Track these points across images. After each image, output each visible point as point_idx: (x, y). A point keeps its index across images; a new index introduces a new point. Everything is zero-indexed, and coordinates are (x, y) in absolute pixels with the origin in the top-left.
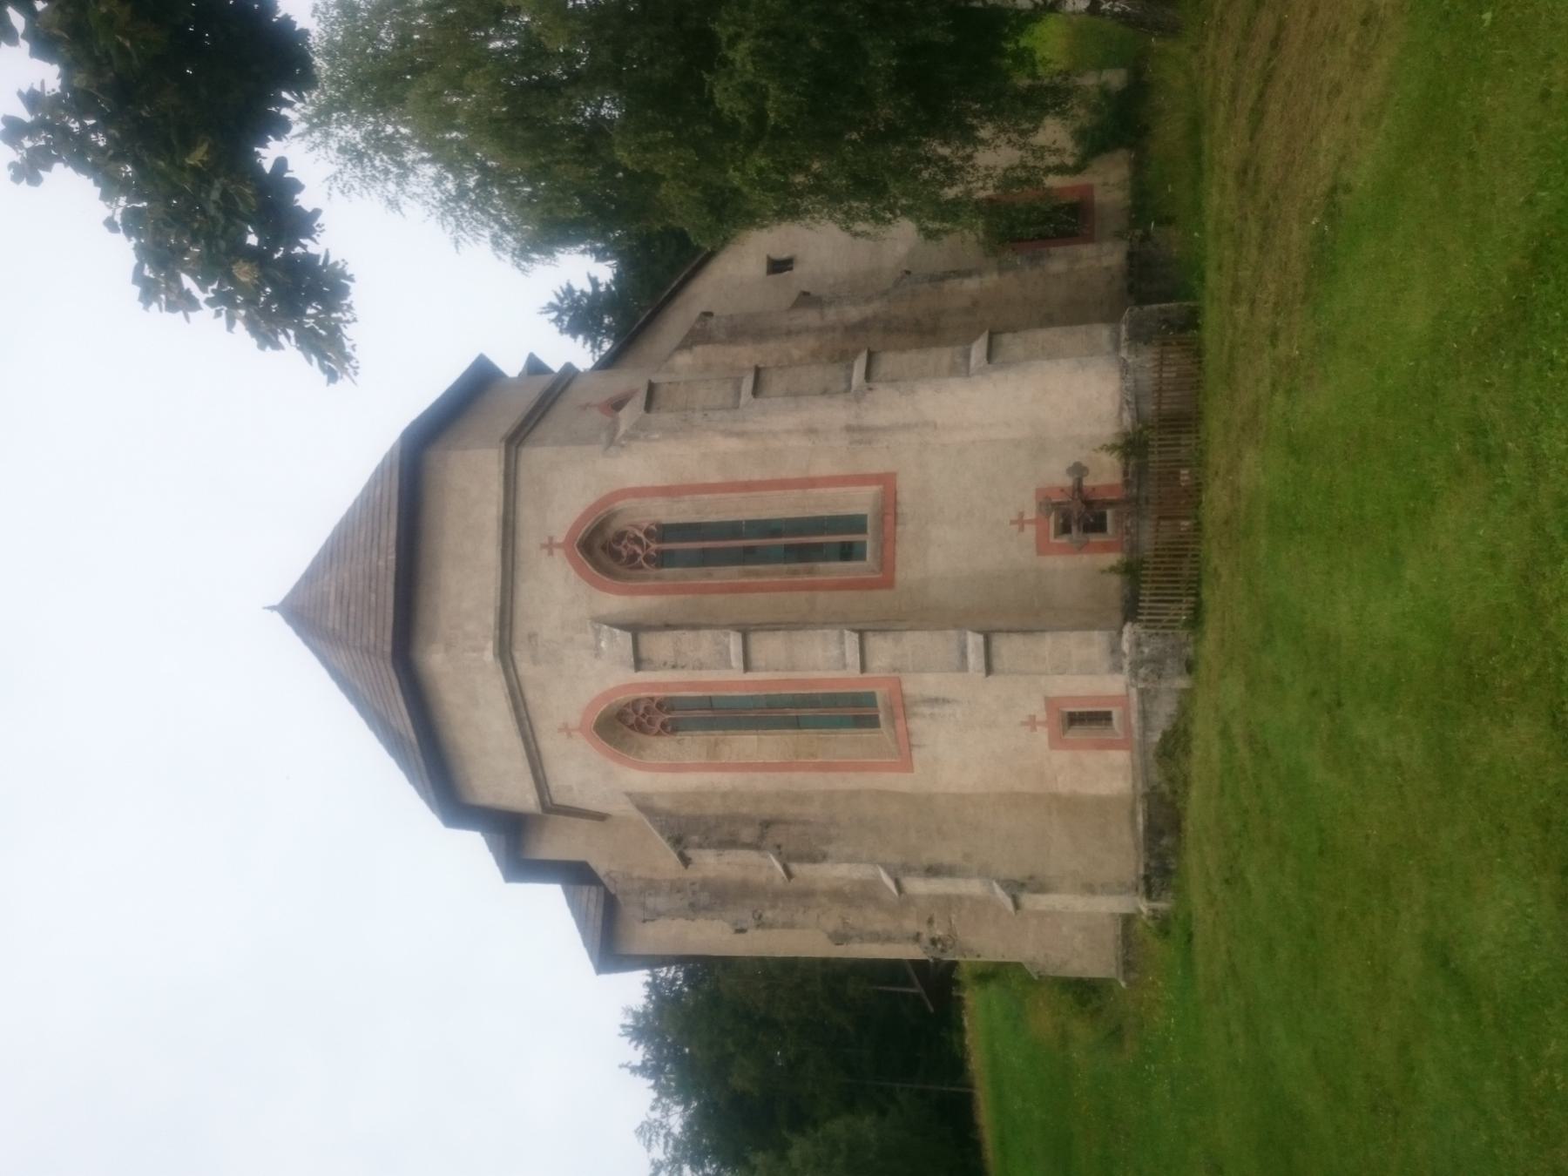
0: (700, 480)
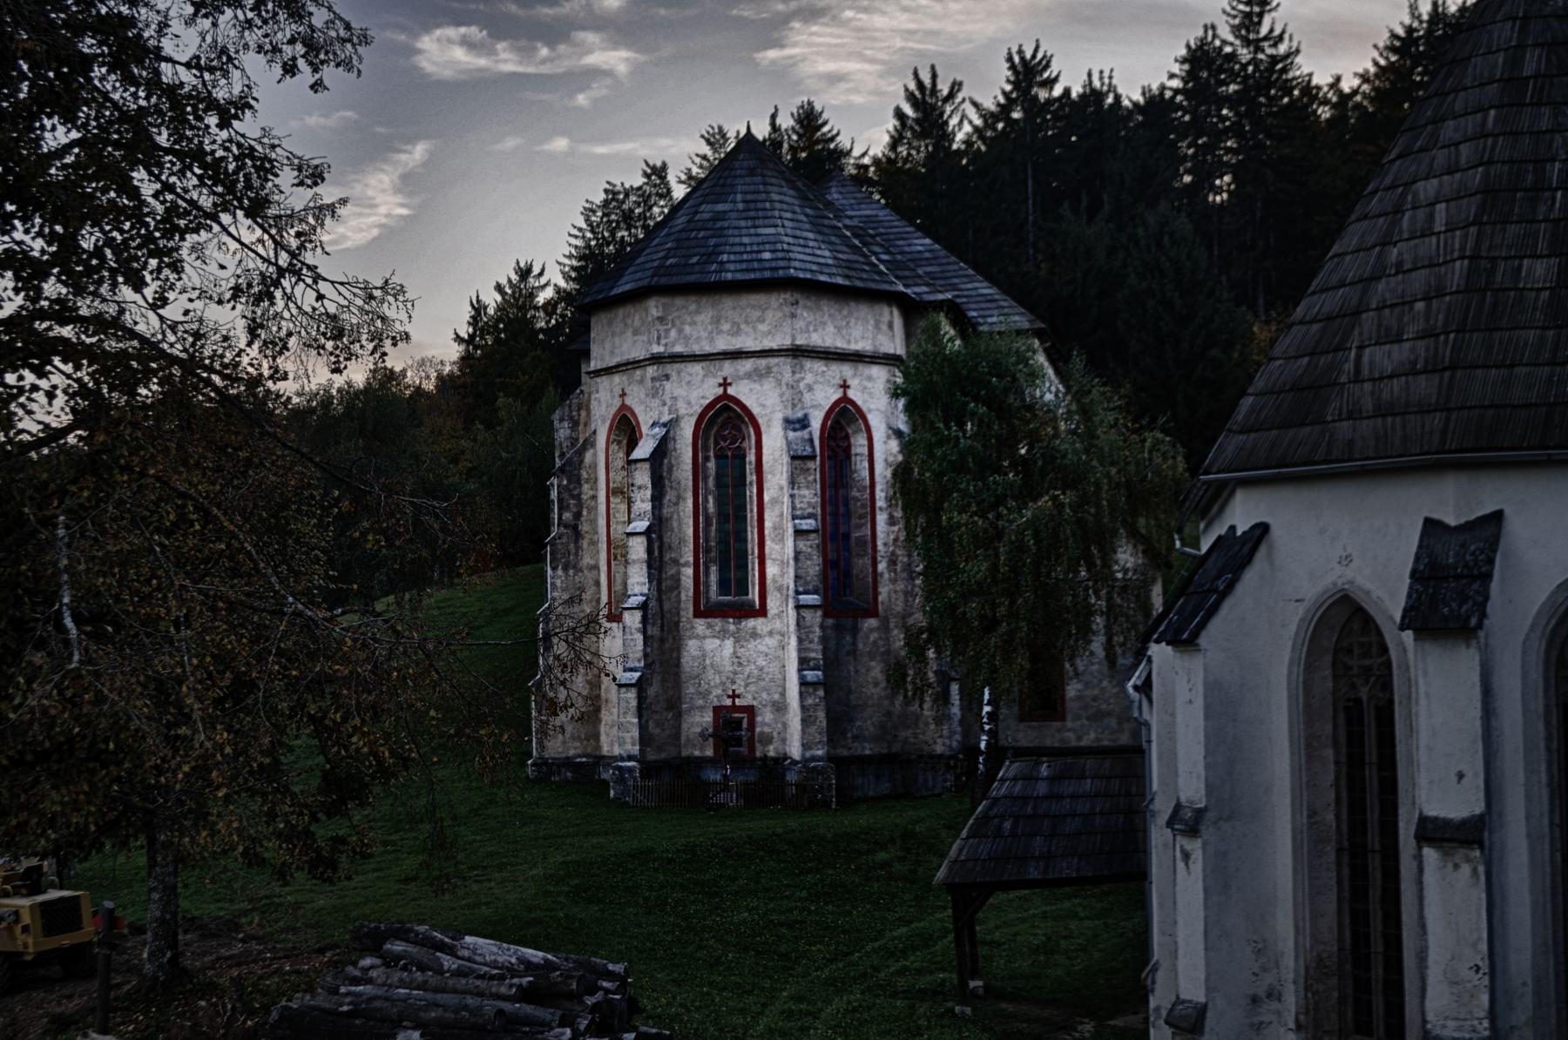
0: (766, 485)
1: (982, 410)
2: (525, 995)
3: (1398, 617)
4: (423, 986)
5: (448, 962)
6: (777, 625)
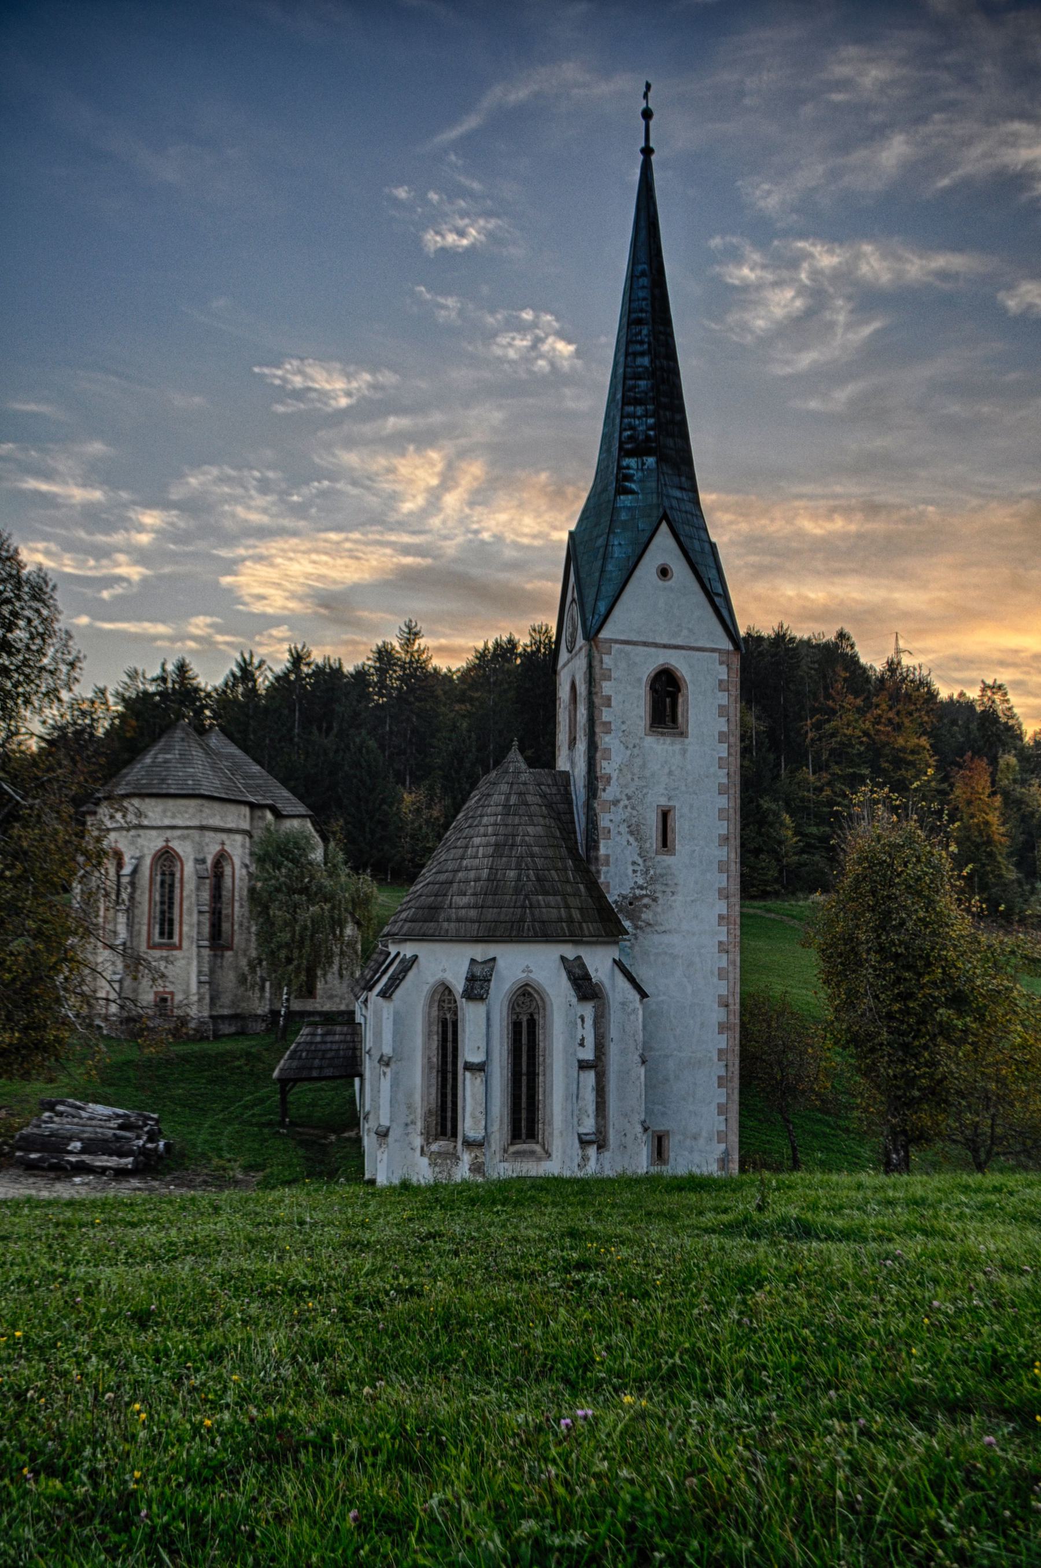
1: (290, 865)
2: (121, 1127)
3: (461, 990)
4: (77, 1124)
5: (84, 1114)
6: (187, 954)
